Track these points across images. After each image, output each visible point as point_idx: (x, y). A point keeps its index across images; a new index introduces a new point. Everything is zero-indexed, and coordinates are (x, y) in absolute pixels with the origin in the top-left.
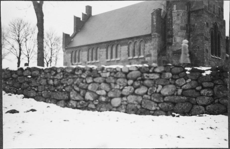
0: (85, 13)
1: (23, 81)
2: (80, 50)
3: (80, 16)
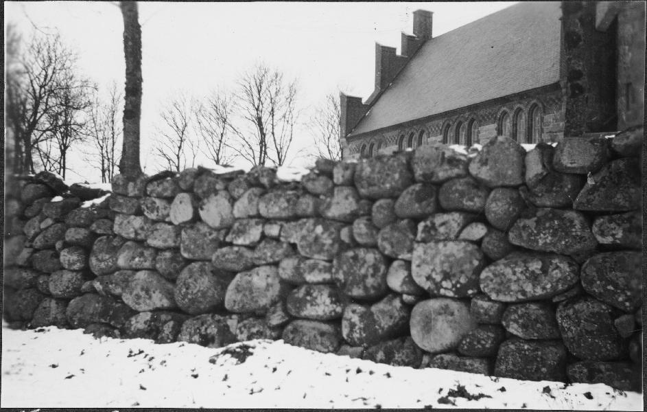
0: (410, 32)
1: (365, 254)
2: (422, 132)
3: (397, 45)
